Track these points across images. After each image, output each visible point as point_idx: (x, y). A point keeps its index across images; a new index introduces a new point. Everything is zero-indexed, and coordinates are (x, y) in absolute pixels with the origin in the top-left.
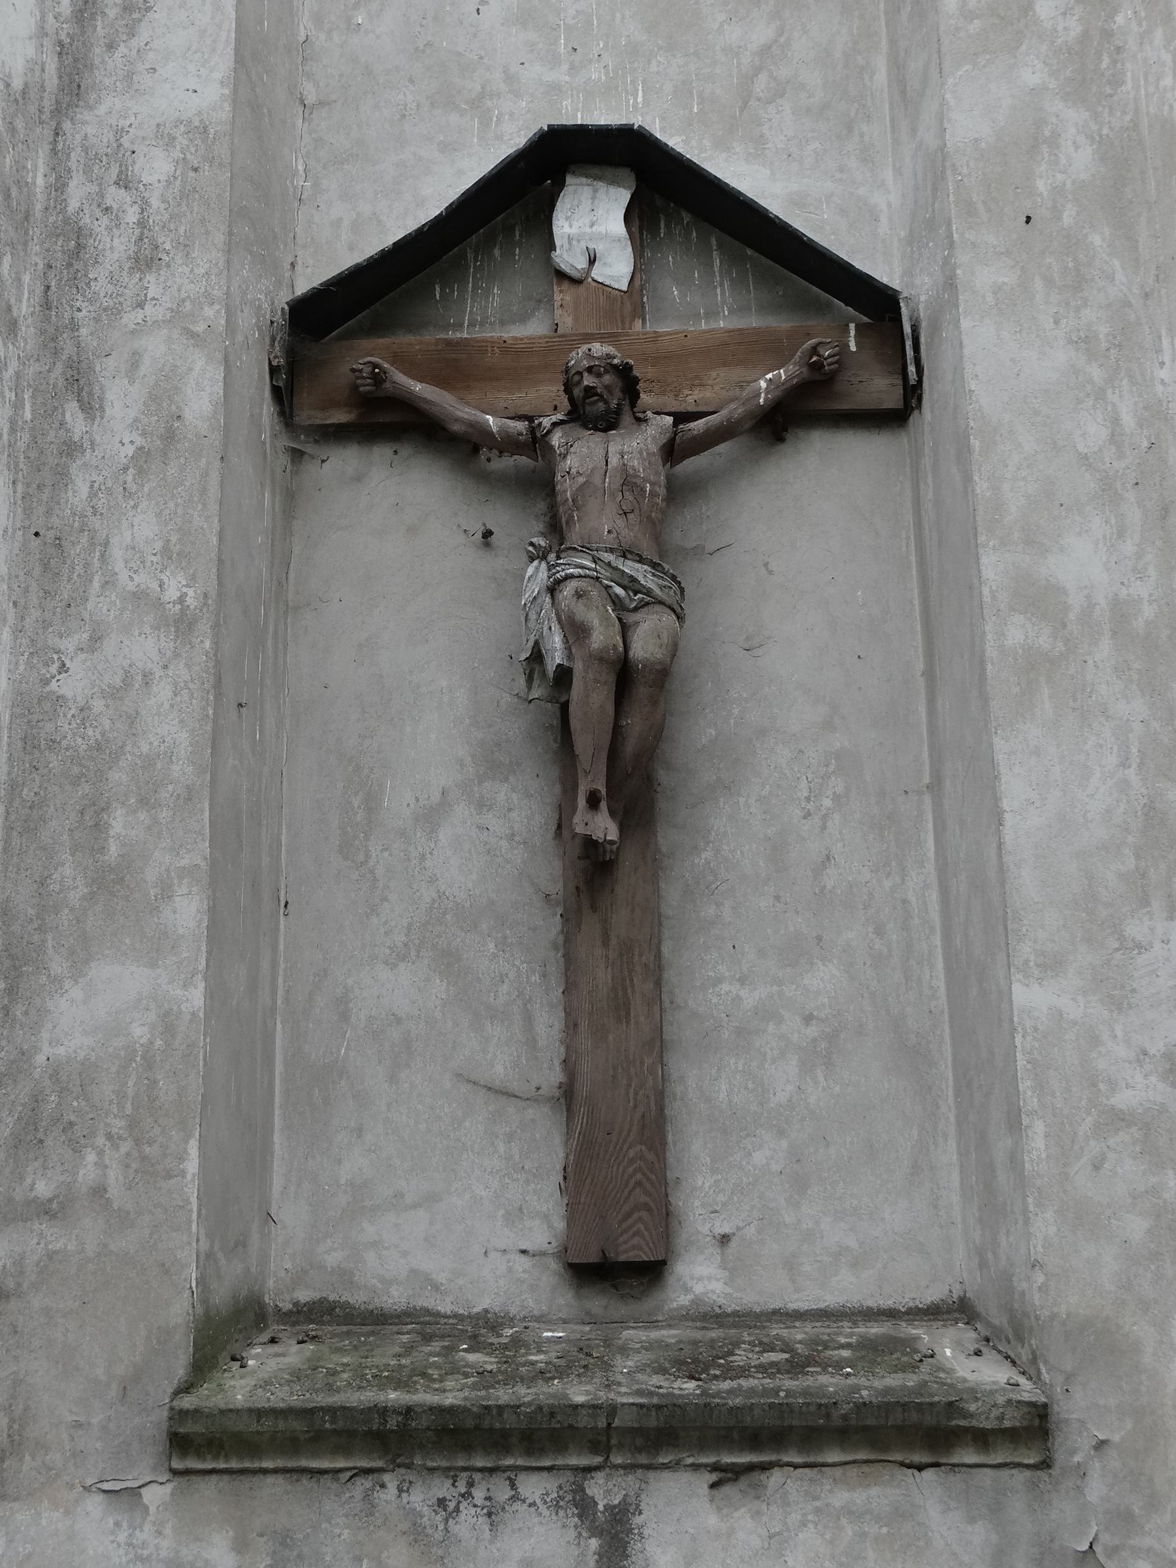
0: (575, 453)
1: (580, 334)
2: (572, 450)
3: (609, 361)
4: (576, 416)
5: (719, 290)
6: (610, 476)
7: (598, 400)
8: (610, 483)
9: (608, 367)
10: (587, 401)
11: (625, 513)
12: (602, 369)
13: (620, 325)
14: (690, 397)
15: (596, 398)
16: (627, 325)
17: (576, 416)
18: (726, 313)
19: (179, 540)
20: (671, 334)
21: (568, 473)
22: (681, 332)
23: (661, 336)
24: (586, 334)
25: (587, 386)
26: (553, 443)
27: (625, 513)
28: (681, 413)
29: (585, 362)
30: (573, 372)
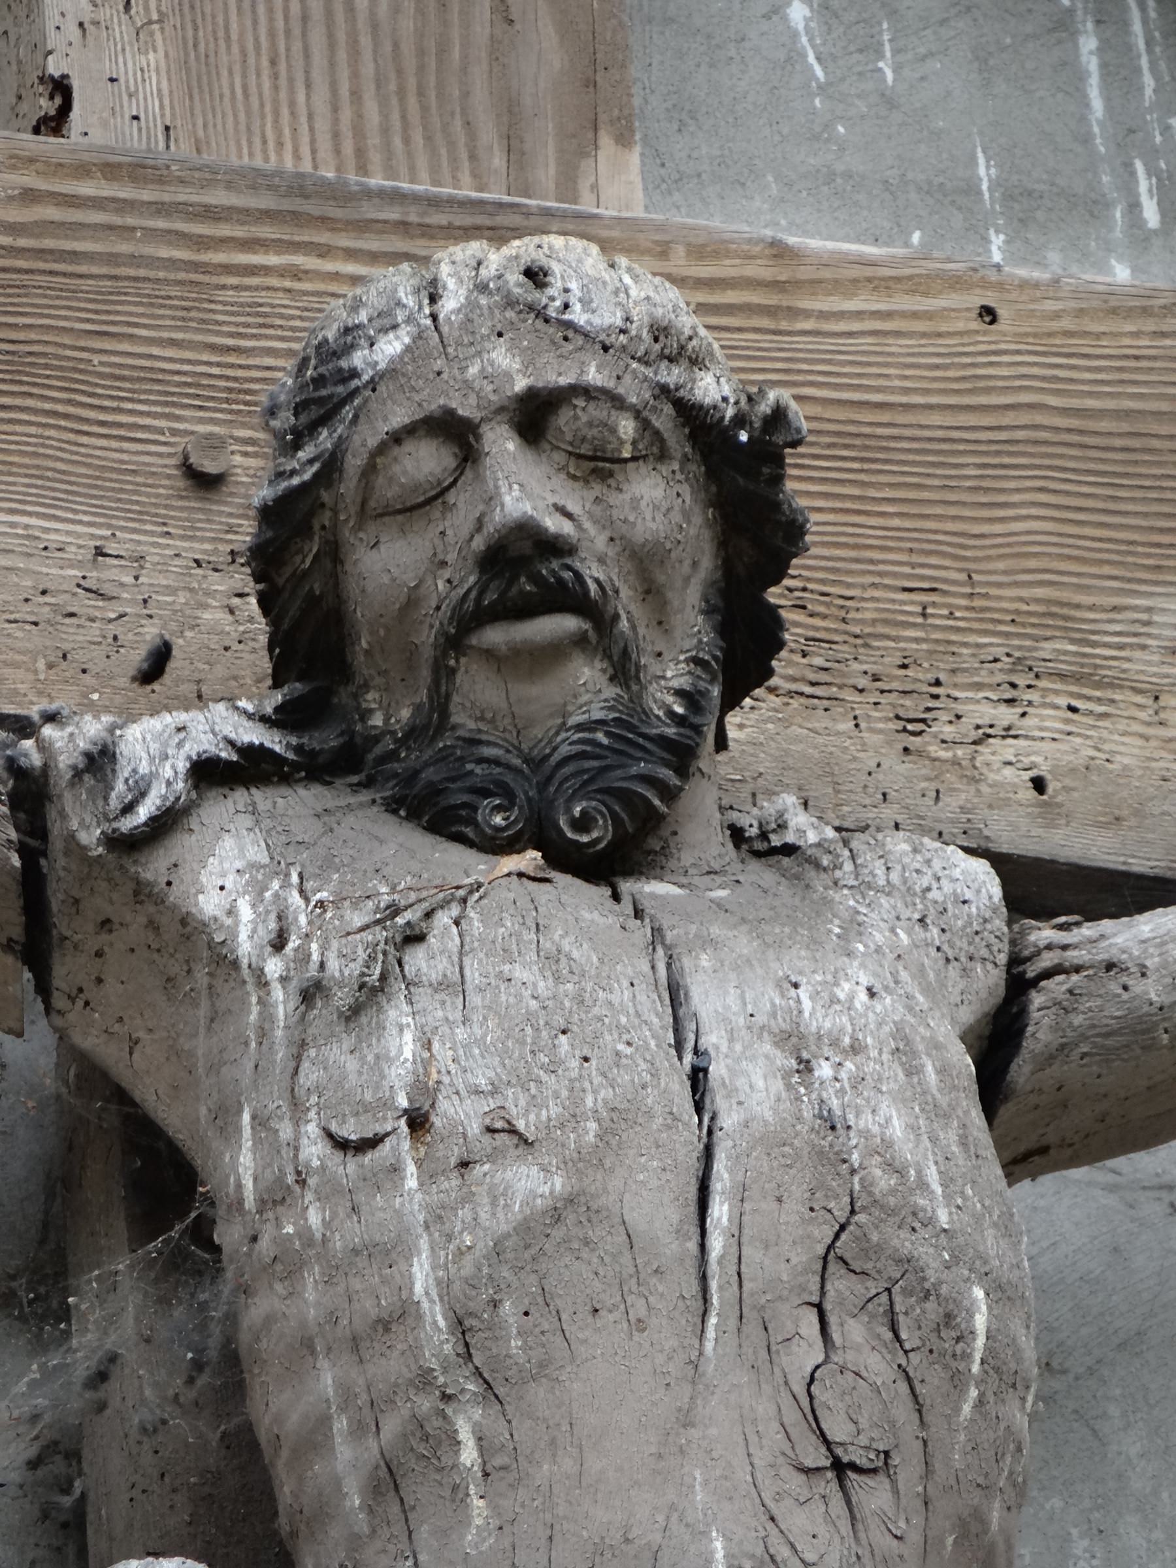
0: (455, 986)
1: (256, 180)
2: (417, 960)
3: (671, 375)
4: (326, 740)
5: (1088, 44)
6: (741, 1194)
7: (580, 641)
8: (737, 1237)
9: (664, 419)
10: (495, 636)
11: (840, 1468)
12: (627, 427)
13: (498, 161)
14: (1007, 749)
15: (569, 623)
16: (546, 173)
17: (326, 740)
18: (1151, 214)
19: (499, 1025)
20: (884, 285)
21: (418, 1122)
22: (956, 283)
23: (814, 285)
24: (299, 187)
25: (526, 530)
26: (209, 904)
27: (840, 1468)
28: (1037, 864)
29: (502, 357)
30: (400, 417)
